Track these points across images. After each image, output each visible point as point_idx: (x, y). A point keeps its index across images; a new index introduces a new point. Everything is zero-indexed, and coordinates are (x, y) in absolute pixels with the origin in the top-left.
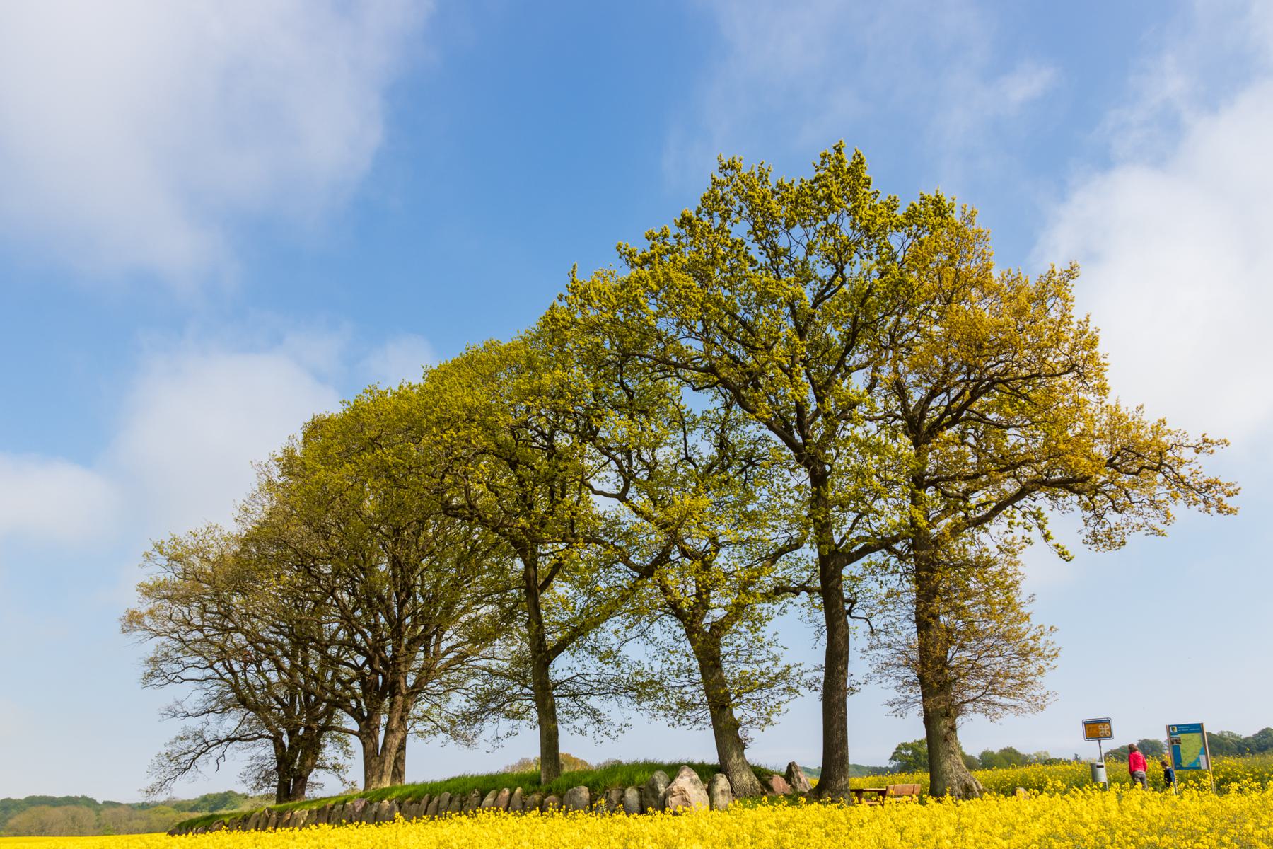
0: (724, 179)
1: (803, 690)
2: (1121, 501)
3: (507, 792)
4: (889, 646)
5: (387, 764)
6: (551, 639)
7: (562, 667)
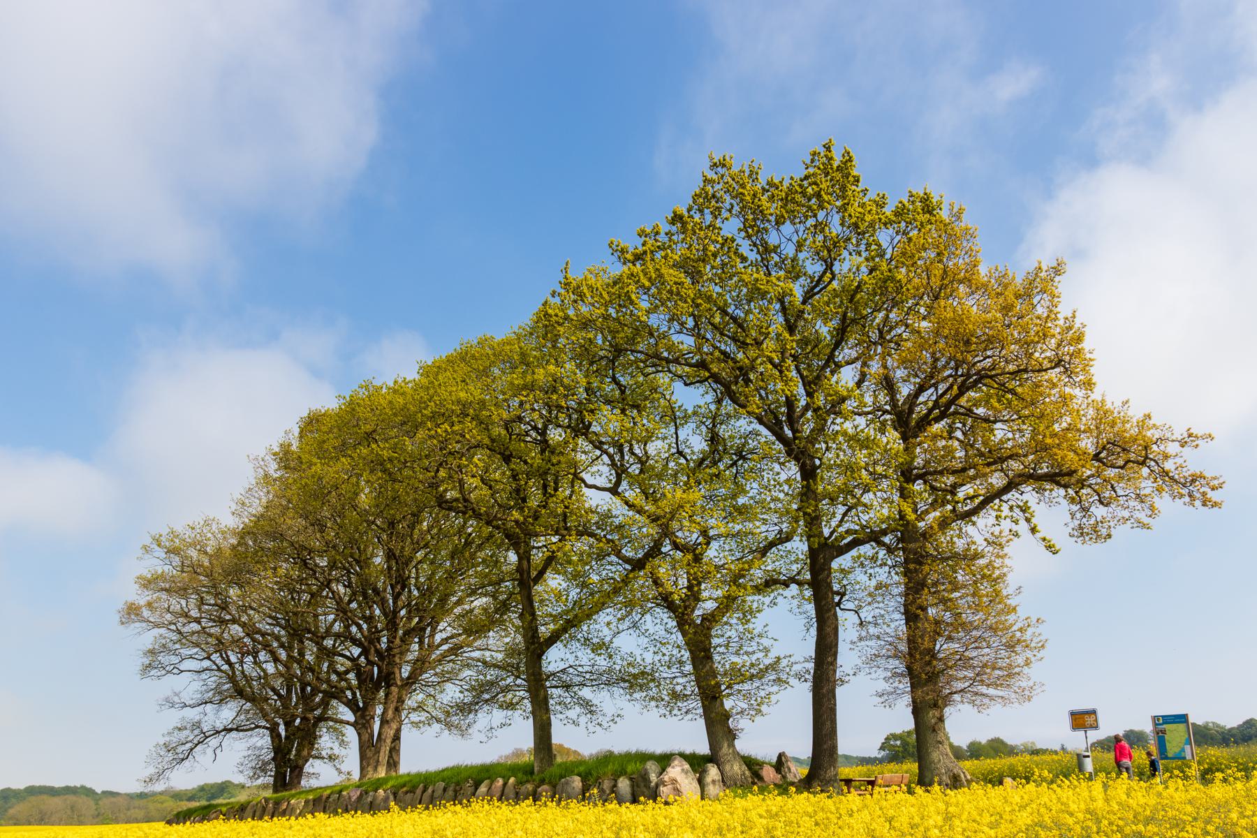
0: (715, 177)
1: (792, 681)
2: (1107, 494)
3: (500, 781)
4: (878, 638)
5: (382, 754)
6: (544, 631)
7: (555, 658)
